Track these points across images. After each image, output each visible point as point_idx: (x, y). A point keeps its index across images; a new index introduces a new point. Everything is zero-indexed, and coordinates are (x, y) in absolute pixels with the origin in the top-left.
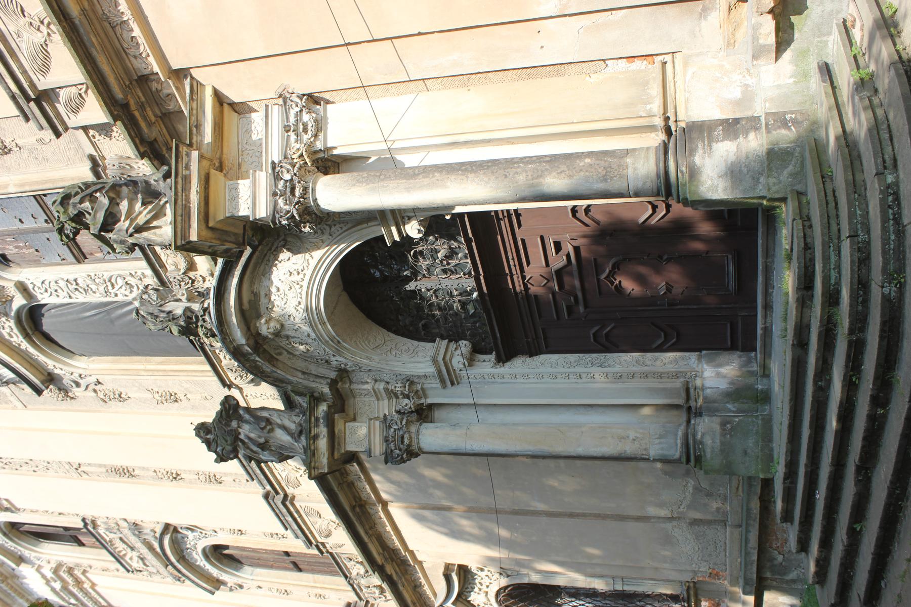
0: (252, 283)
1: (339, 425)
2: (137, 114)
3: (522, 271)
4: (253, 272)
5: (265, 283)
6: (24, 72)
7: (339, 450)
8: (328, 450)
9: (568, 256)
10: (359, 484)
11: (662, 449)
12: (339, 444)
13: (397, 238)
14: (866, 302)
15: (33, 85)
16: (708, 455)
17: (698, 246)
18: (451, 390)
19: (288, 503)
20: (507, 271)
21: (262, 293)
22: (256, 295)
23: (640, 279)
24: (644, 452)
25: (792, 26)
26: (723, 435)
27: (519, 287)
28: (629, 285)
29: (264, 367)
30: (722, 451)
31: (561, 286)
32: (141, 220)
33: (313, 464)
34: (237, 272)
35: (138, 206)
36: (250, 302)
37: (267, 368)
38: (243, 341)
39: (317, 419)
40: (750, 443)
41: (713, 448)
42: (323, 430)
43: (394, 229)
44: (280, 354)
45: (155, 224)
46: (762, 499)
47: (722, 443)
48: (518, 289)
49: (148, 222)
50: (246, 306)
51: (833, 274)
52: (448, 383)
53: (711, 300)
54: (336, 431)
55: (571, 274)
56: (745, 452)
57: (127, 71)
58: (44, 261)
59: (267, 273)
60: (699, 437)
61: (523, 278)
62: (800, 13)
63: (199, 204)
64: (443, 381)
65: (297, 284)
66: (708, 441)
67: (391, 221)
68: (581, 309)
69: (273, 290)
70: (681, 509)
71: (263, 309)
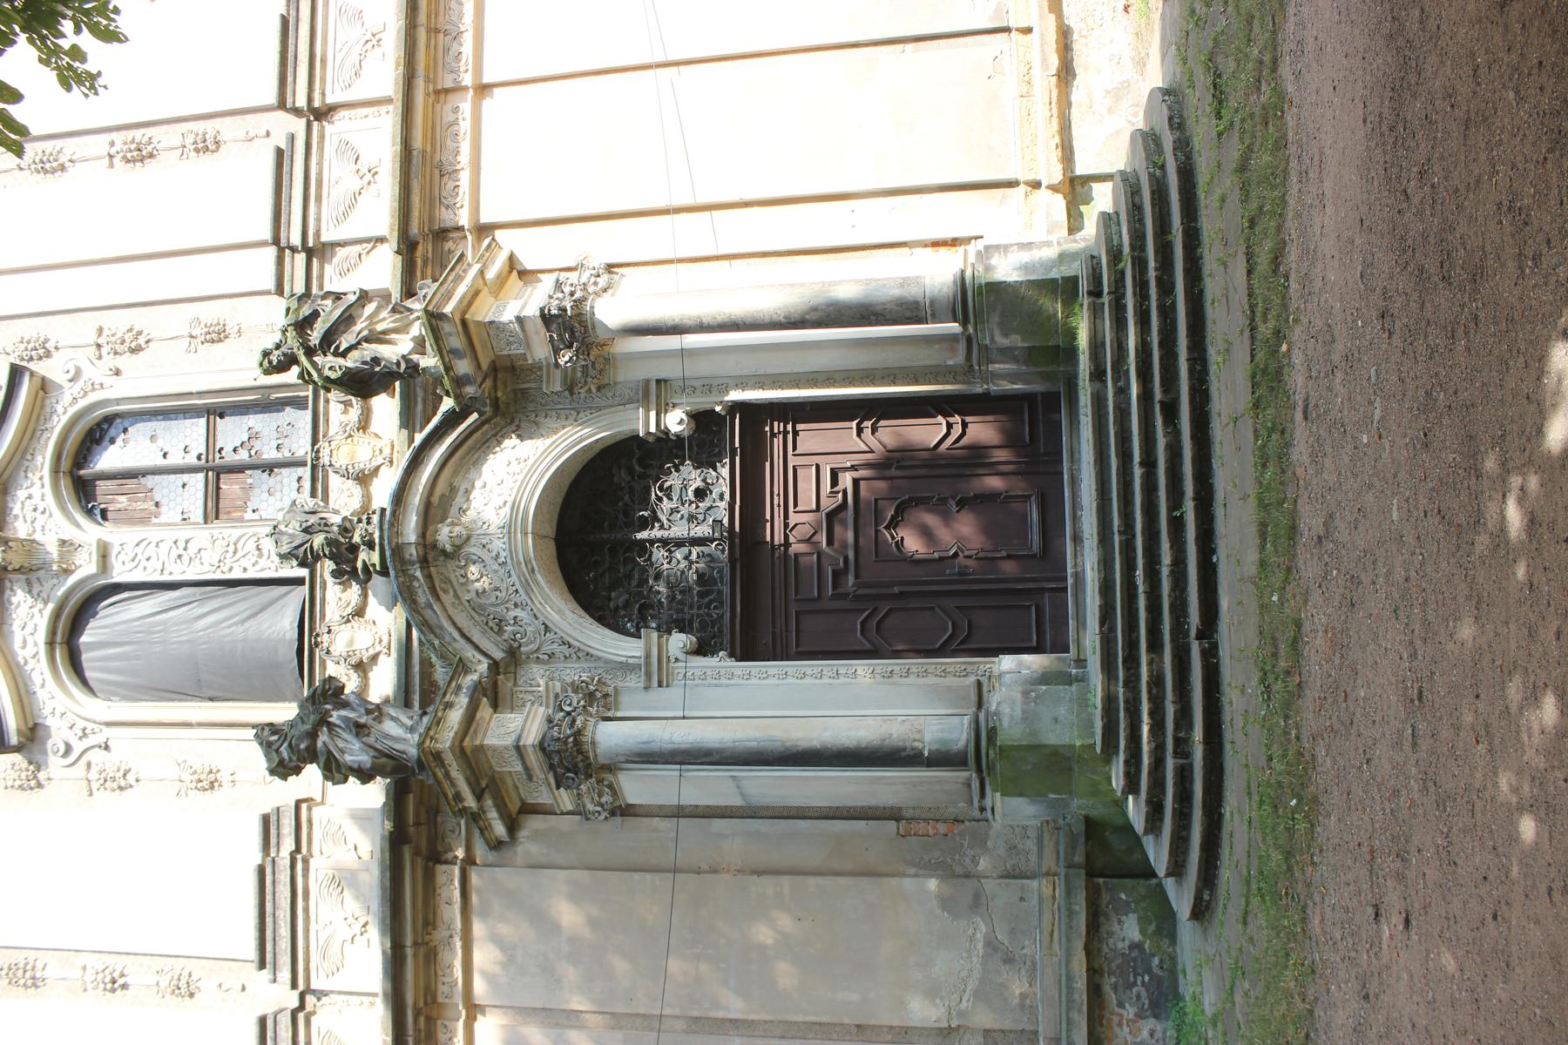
0: (455, 473)
1: (485, 710)
2: (419, 262)
3: (786, 516)
4: (467, 453)
5: (472, 475)
6: (318, 220)
7: (472, 740)
8: (461, 723)
9: (845, 492)
10: (444, 955)
11: (942, 731)
12: (475, 732)
13: (653, 429)
14: (1141, 220)
15: (318, 234)
16: (1006, 724)
17: (995, 483)
18: (658, 694)
19: (301, 1016)
20: (768, 517)
21: (462, 489)
22: (453, 490)
23: (926, 533)
24: (917, 736)
25: (1081, 215)
26: (1024, 703)
27: (779, 538)
28: (913, 544)
29: (420, 591)
30: (1024, 719)
31: (830, 542)
32: (380, 327)
33: (432, 733)
34: (449, 440)
35: (384, 314)
36: (443, 496)
37: (423, 596)
38: (412, 538)
39: (459, 687)
40: (1062, 710)
41: (1012, 717)
42: (463, 700)
43: (653, 414)
44: (445, 591)
45: (393, 336)
46: (1089, 952)
47: (1024, 712)
48: (776, 542)
49: (384, 332)
50: (435, 500)
51: (1115, 238)
52: (655, 684)
53: (1009, 568)
54: (478, 715)
55: (844, 523)
56: (1056, 720)
57: (431, 219)
58: (154, 520)
59: (478, 463)
60: (993, 708)
61: (786, 525)
62: (1088, 203)
63: (463, 297)
64: (648, 675)
65: (513, 479)
66: (1006, 709)
67: (653, 405)
68: (851, 579)
69: (478, 484)
70: (964, 1004)
71: (453, 511)
